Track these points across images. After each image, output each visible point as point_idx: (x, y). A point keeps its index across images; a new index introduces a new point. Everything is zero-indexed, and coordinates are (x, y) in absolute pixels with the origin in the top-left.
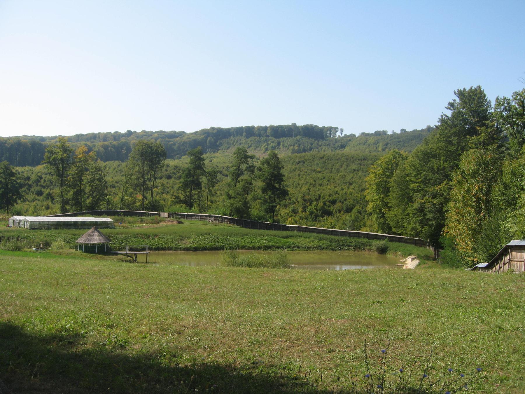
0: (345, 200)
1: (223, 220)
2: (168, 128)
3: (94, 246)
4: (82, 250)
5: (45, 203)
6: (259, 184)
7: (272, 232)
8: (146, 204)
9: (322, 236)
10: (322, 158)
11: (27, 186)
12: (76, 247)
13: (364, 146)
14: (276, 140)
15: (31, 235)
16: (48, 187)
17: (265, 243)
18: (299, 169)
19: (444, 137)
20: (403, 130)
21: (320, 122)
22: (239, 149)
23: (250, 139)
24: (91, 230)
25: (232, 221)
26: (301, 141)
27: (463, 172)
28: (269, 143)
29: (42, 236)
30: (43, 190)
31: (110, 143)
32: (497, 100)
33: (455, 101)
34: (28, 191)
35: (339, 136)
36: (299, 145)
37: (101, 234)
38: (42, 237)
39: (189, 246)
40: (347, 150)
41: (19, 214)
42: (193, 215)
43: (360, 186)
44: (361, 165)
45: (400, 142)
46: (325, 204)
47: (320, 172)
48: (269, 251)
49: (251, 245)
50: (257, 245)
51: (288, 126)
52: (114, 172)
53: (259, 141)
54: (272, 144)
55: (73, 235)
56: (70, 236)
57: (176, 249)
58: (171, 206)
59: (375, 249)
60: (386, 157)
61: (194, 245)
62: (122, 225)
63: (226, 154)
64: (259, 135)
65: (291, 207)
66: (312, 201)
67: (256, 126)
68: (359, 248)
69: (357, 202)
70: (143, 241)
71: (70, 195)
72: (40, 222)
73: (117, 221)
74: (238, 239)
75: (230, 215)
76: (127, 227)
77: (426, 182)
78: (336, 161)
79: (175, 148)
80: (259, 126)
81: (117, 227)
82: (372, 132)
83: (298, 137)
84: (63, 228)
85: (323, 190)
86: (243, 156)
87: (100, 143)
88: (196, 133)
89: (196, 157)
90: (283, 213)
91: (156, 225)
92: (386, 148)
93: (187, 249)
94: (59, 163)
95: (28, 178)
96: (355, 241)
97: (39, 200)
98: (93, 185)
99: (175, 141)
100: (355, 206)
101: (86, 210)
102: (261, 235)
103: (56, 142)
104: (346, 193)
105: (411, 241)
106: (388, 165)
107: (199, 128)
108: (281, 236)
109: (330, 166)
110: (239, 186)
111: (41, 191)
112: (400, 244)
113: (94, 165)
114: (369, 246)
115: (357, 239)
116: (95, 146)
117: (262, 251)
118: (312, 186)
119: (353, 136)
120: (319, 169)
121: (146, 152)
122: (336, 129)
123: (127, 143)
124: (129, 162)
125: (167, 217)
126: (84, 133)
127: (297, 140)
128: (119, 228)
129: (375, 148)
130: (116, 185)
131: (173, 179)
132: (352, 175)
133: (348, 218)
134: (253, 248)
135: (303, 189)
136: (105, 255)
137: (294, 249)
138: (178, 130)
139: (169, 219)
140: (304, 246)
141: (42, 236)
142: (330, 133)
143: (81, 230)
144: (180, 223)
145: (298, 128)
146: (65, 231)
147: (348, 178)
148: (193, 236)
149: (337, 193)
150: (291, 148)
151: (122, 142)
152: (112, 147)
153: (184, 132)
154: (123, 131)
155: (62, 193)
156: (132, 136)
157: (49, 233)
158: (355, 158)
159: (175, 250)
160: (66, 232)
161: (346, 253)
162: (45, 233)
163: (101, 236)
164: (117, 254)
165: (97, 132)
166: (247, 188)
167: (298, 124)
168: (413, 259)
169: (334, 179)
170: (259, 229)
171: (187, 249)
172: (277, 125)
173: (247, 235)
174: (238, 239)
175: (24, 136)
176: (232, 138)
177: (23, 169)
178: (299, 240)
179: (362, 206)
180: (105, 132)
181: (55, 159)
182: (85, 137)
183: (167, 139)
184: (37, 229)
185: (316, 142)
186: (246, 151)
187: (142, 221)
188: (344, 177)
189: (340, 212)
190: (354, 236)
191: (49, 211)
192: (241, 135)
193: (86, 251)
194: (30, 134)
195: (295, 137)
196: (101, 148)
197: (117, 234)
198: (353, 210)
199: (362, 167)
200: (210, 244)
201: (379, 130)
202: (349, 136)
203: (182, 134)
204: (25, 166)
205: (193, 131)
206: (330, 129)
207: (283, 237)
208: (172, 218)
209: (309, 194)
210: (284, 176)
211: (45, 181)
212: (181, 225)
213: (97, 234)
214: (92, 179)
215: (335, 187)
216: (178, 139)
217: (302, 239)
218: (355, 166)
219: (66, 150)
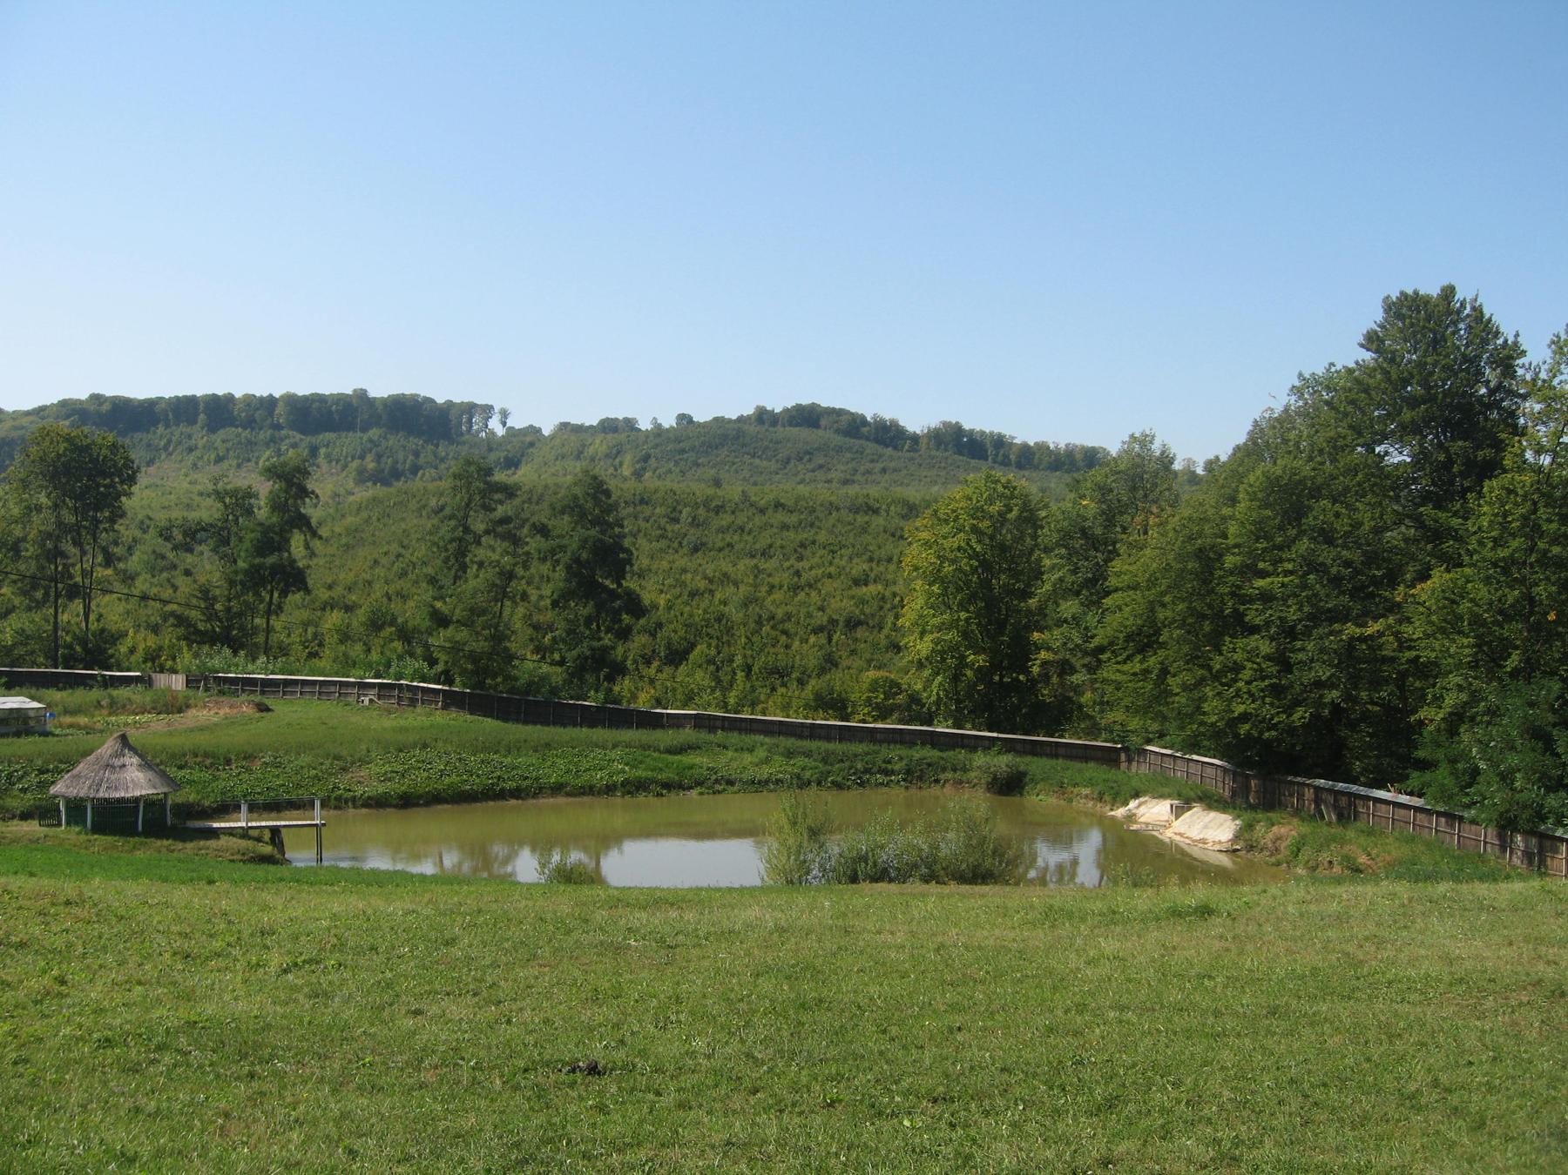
1: (413, 697)
6: (544, 583)
7: (600, 734)
20: (684, 419)
25: (452, 701)
28: (284, 448)
36: (379, 457)
39: (380, 790)
42: (287, 683)
45: (683, 451)
48: (641, 798)
49: (580, 782)
51: (340, 399)
53: (250, 442)
61: (395, 787)
67: (238, 395)
68: (920, 778)
69: (696, 632)
70: (215, 778)
82: (592, 420)
83: (374, 433)
92: (644, 469)
96: (901, 759)
100: (693, 646)
107: (50, 397)
110: (475, 582)
117: (617, 800)
119: (534, 431)
122: (487, 410)
134: (589, 790)
136: (184, 841)
140: (745, 777)
150: (355, 464)
159: (336, 808)
164: (214, 834)
171: (377, 803)
176: (161, 429)
185: (430, 447)
187: (115, 707)
189: (648, 663)
192: (192, 421)
193: (98, 829)
195: (364, 430)
199: (643, 525)
200: (447, 780)
206: (470, 408)
207: (670, 751)
208: (201, 693)
213: (135, 760)
217: (730, 754)
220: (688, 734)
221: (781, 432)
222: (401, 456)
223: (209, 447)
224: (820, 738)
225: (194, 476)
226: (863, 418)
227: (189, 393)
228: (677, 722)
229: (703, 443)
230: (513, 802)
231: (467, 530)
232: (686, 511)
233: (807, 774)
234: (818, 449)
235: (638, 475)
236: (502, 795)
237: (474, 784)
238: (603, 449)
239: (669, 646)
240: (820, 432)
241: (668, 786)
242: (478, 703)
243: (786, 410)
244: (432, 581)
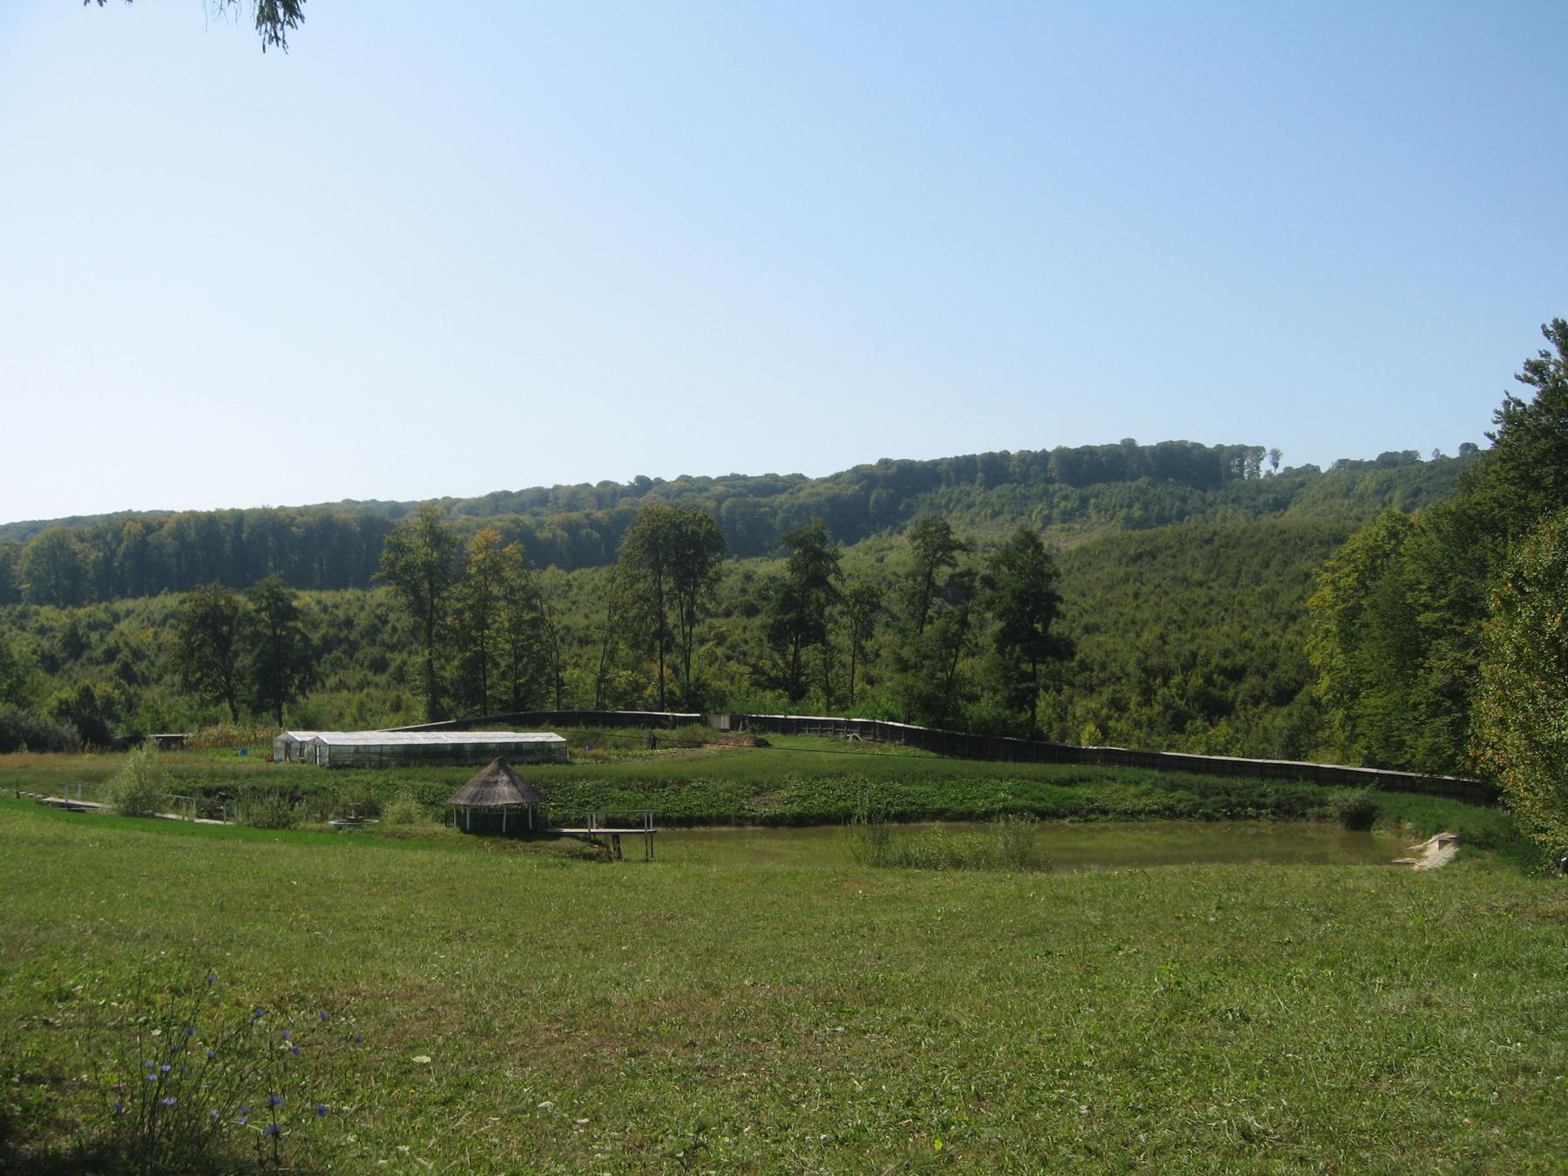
0: (1273, 666)
1: (894, 734)
2: (755, 467)
5: (393, 694)
10: (1209, 541)
11: (344, 646)
12: (446, 819)
13: (1346, 502)
14: (1075, 493)
15: (329, 783)
16: (404, 646)
17: (1005, 800)
18: (1139, 578)
19: (1513, 468)
20: (1466, 447)
25: (912, 738)
27: (1518, 575)
29: (353, 788)
30: (388, 655)
31: (588, 516)
33: (1547, 355)
34: (346, 660)
35: (1269, 474)
36: (1145, 507)
38: (358, 791)
41: (309, 725)
46: (1209, 680)
47: (1200, 584)
49: (961, 808)
50: (981, 805)
51: (1110, 450)
52: (582, 600)
53: (1024, 496)
54: (1063, 503)
55: (447, 782)
56: (438, 785)
57: (741, 821)
60: (1373, 530)
61: (796, 808)
62: (594, 751)
65: (1107, 692)
67: (1013, 451)
76: (605, 759)
79: (777, 523)
80: (1022, 452)
82: (1371, 455)
83: (1143, 481)
85: (1207, 638)
87: (557, 518)
88: (836, 478)
89: (806, 551)
90: (1079, 712)
92: (1414, 504)
93: (773, 822)
95: (349, 623)
96: (1277, 791)
97: (377, 685)
102: (995, 777)
107: (845, 465)
108: (1053, 777)
111: (383, 658)
112: (1413, 797)
116: (540, 525)
120: (1198, 576)
122: (1258, 452)
126: (514, 488)
127: (1138, 489)
132: (1298, 589)
133: (1279, 720)
134: (969, 816)
135: (1145, 636)
137: (1093, 816)
138: (783, 472)
139: (732, 734)
140: (1120, 808)
141: (353, 788)
142: (1241, 466)
146: (428, 771)
147: (1284, 602)
149: (1246, 646)
150: (1122, 513)
153: (801, 477)
154: (625, 479)
156: (651, 494)
159: (737, 825)
162: (369, 778)
163: (515, 785)
168: (1443, 843)
169: (1241, 603)
170: (992, 759)
171: (773, 822)
172: (760, 473)
173: (951, 777)
175: (347, 502)
176: (943, 489)
177: (338, 599)
178: (1107, 791)
180: (573, 484)
181: (409, 568)
183: (751, 498)
186: (948, 528)
188: (1271, 596)
189: (1256, 704)
190: (1274, 777)
192: (971, 481)
194: (361, 495)
195: (1133, 479)
196: (559, 532)
197: (573, 778)
198: (1298, 697)
200: (841, 804)
202: (1299, 472)
204: (346, 588)
205: (827, 474)
206: (1240, 452)
209: (1161, 652)
210: (1061, 600)
211: (394, 629)
212: (764, 751)
213: (505, 778)
215: (1244, 628)
216: (785, 496)
217: (1116, 786)
222: (1168, 504)
223: (985, 504)
224: (1215, 773)
227: (968, 453)
238: (1373, 485)
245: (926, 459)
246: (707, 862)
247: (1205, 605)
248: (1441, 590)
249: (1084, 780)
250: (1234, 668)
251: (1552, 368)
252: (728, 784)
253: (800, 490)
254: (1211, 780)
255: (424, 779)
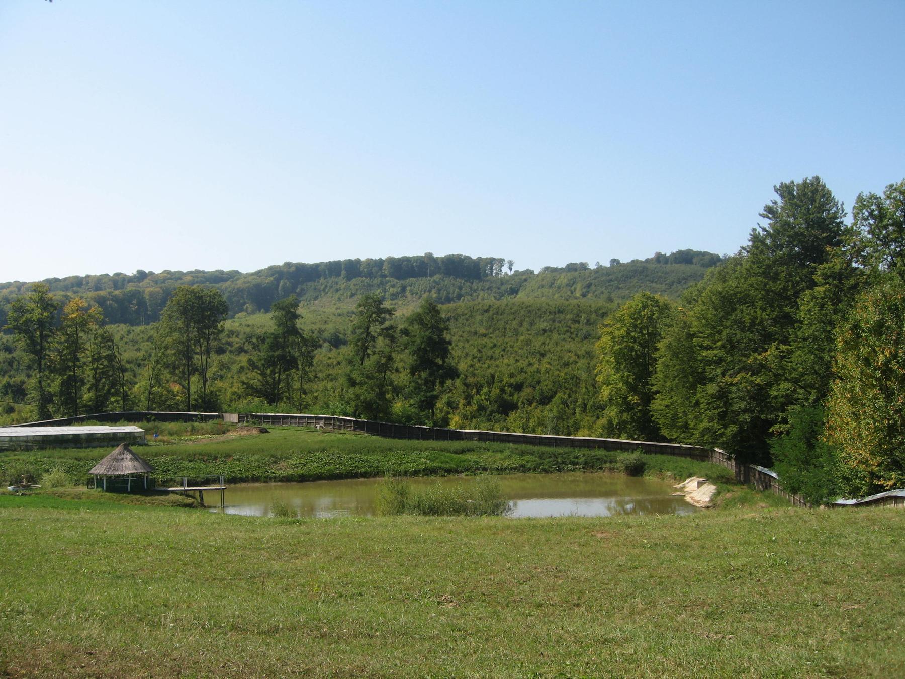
0: (539, 382)
1: (341, 424)
2: (209, 266)
3: (123, 479)
4: (102, 487)
6: (404, 359)
8: (195, 400)
9: (523, 447)
10: (487, 311)
12: (89, 483)
17: (426, 463)
20: (614, 261)
21: (474, 249)
22: (367, 298)
23: (354, 281)
24: (117, 450)
25: (358, 426)
26: (442, 283)
29: (20, 462)
31: (109, 293)
32: (860, 198)
33: (775, 203)
35: (506, 274)
36: (439, 291)
37: (135, 457)
40: (521, 296)
43: (560, 358)
44: (554, 321)
45: (611, 280)
46: (502, 390)
47: (485, 336)
50: (412, 466)
51: (418, 259)
52: (133, 342)
54: (391, 289)
55: (76, 459)
57: (267, 479)
58: (231, 401)
59: (622, 467)
61: (300, 471)
62: (160, 437)
63: (312, 308)
64: (370, 275)
66: (481, 386)
67: (363, 259)
68: (592, 467)
69: (558, 385)
70: (207, 467)
71: (55, 386)
72: (11, 437)
73: (147, 431)
74: (375, 457)
75: (354, 416)
76: (169, 443)
77: (731, 346)
78: (511, 317)
80: (368, 259)
81: (152, 443)
82: (562, 265)
83: (437, 277)
84: (54, 448)
86: (375, 310)
87: (91, 294)
88: (259, 273)
91: (221, 437)
92: (588, 292)
93: (287, 479)
94: (35, 330)
96: (584, 455)
98: (97, 368)
99: (223, 287)
100: (555, 393)
101: (87, 412)
102: (417, 449)
103: (11, 292)
104: (538, 371)
105: (697, 452)
106: (636, 319)
107: (264, 265)
109: (501, 325)
113: (100, 332)
114: (611, 462)
115: (586, 451)
117: (420, 478)
118: (475, 360)
119: (529, 272)
121: (192, 307)
122: (501, 261)
123: (139, 292)
124: (162, 324)
125: (236, 420)
127: (435, 281)
128: (155, 444)
129: (569, 293)
130: (128, 366)
131: (228, 353)
133: (549, 412)
138: (226, 269)
140: (494, 466)
141: (20, 462)
143: (88, 450)
144: (264, 431)
145: (435, 260)
147: (537, 344)
148: (295, 455)
149: (522, 370)
150: (425, 296)
151: (130, 291)
152: (112, 300)
153: (237, 272)
154: (130, 271)
155: (40, 382)
156: (146, 280)
157: (30, 457)
158: (544, 310)
159: (265, 482)
160: (62, 454)
161: (569, 477)
163: (137, 460)
164: (167, 493)
165: (83, 275)
166: (385, 365)
167: (436, 255)
168: (700, 484)
171: (287, 479)
172: (400, 256)
173: (390, 450)
174: (375, 457)
176: (322, 280)
178: (485, 457)
179: (567, 392)
181: (28, 321)
182: (61, 283)
184: (7, 450)
187: (194, 431)
188: (528, 343)
189: (530, 404)
190: (580, 447)
191: (14, 416)
192: (338, 274)
193: (109, 490)
195: (431, 276)
197: (157, 455)
198: (554, 400)
199: (557, 325)
200: (327, 468)
201: (573, 262)
202: (523, 273)
203: (234, 275)
205: (253, 270)
206: (491, 261)
207: (456, 452)
208: (245, 424)
213: (129, 456)
214: (96, 356)
215: (517, 361)
216: (228, 283)
217: (489, 453)
218: (545, 324)
219: (48, 305)
220: (475, 443)
221: (669, 267)
225: (338, 305)
226: (718, 256)
228: (469, 436)
229: (623, 276)
230: (362, 480)
231: (368, 334)
232: (583, 316)
233: (529, 465)
234: (690, 276)
235: (584, 295)
236: (356, 476)
237: (343, 469)
239: (542, 394)
240: (692, 266)
241: (449, 471)
242: (370, 428)
243: (673, 254)
244: (350, 362)
245: (311, 263)
246: (858, 513)
247: (492, 348)
248: (717, 337)
249: (469, 450)
250: (517, 384)
251: (780, 210)
252: (256, 457)
253: (237, 279)
254: (530, 447)
255: (61, 457)
